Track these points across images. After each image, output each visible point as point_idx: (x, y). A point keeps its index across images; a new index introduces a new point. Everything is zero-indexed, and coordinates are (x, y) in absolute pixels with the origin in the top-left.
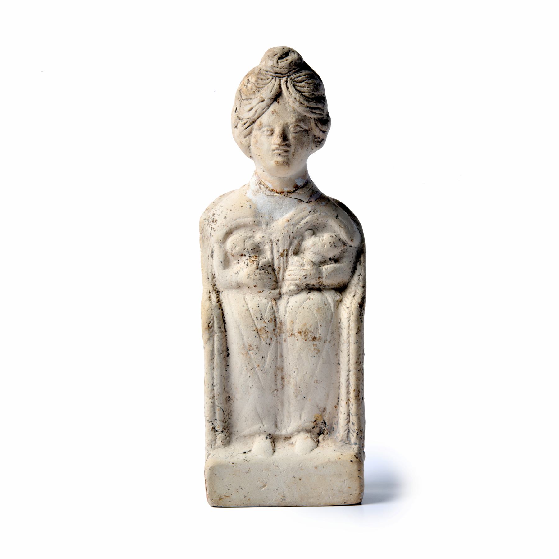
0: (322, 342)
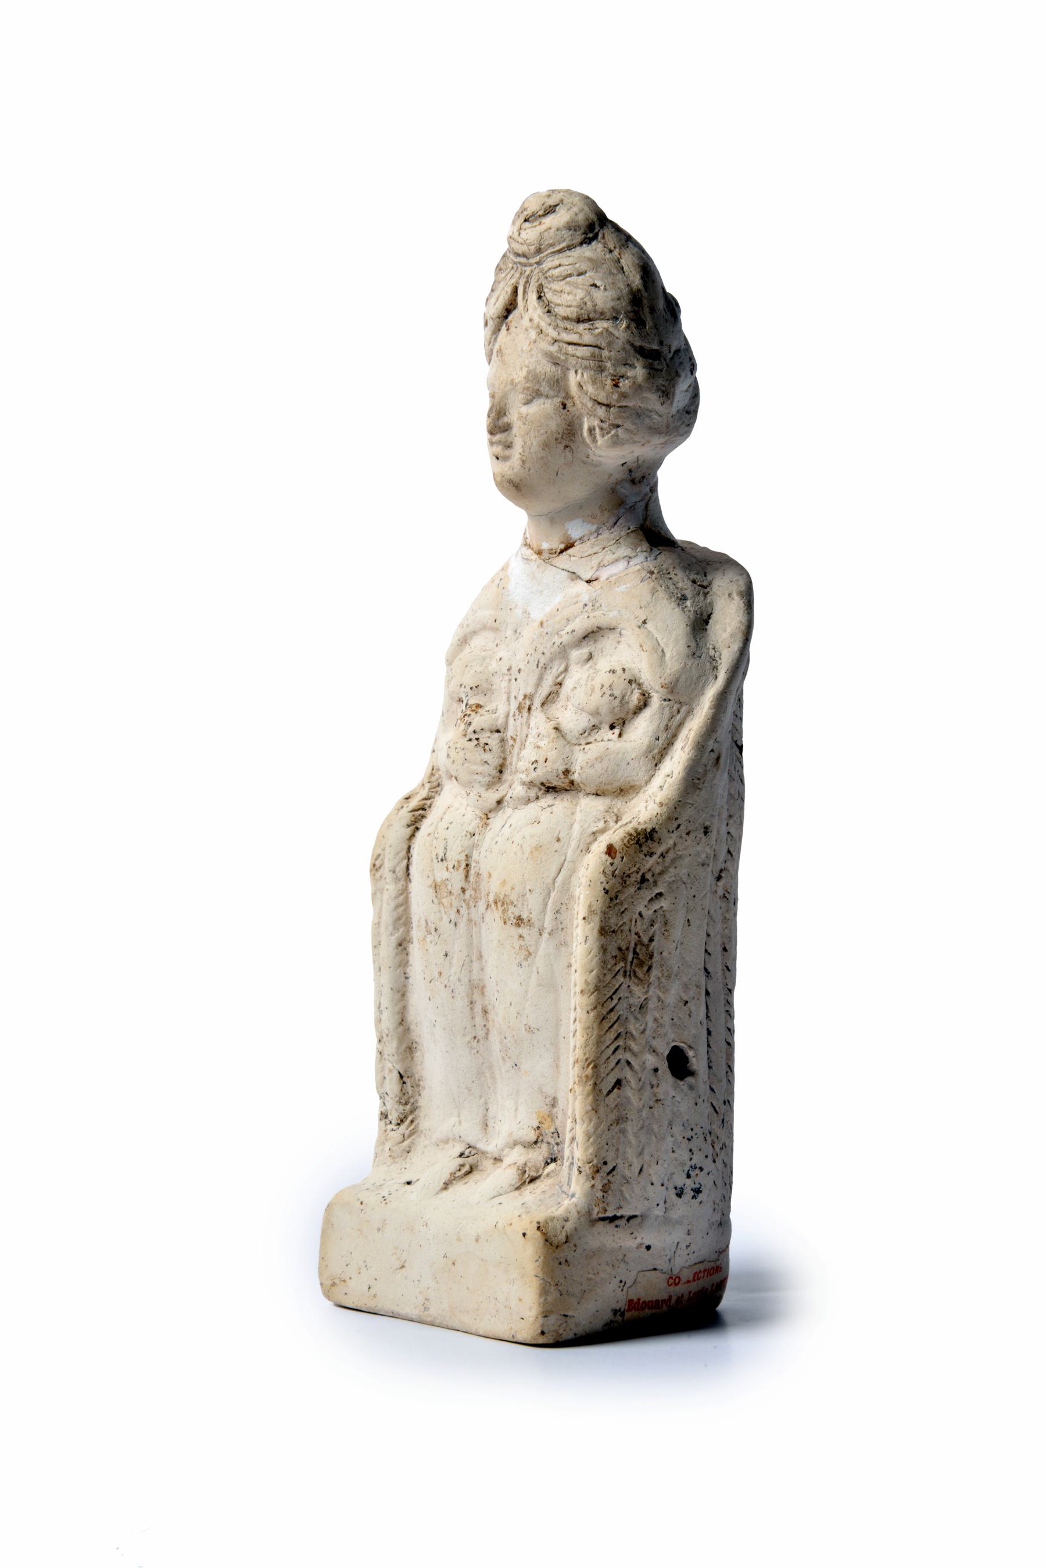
0: (535, 931)
